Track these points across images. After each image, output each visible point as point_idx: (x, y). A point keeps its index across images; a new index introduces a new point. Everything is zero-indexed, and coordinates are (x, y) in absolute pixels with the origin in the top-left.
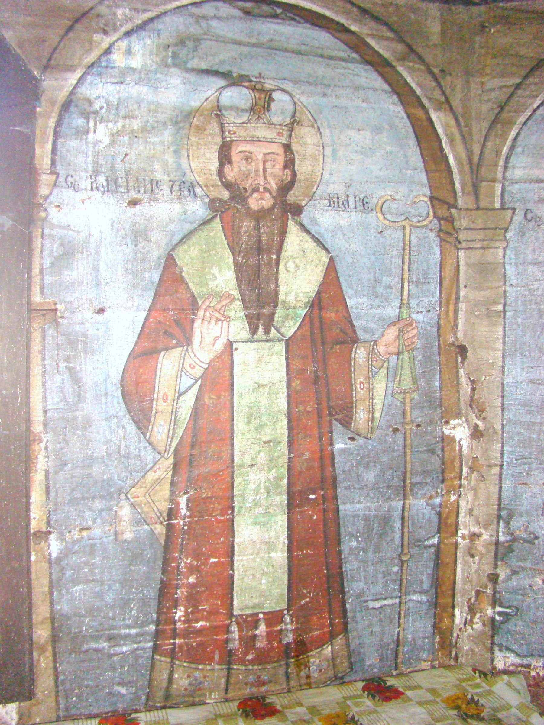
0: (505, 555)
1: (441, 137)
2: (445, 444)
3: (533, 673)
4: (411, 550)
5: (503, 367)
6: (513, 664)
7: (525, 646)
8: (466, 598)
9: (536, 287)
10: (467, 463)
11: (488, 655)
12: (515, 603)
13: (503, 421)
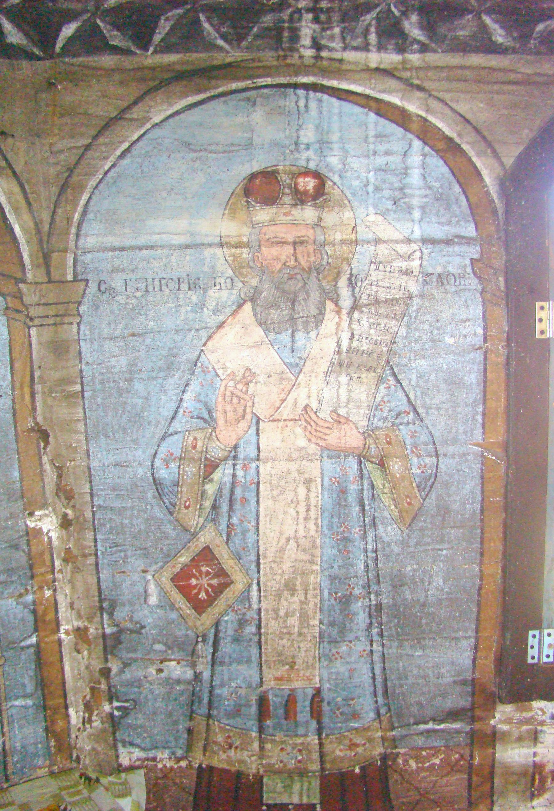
0: (114, 647)
1: (4, 206)
2: (31, 538)
3: (160, 766)
4: (5, 653)
5: (88, 451)
6: (139, 759)
7: (148, 739)
8: (80, 696)
9: (113, 363)
10: (59, 555)
11: (112, 753)
12: (132, 697)
13: (93, 508)
